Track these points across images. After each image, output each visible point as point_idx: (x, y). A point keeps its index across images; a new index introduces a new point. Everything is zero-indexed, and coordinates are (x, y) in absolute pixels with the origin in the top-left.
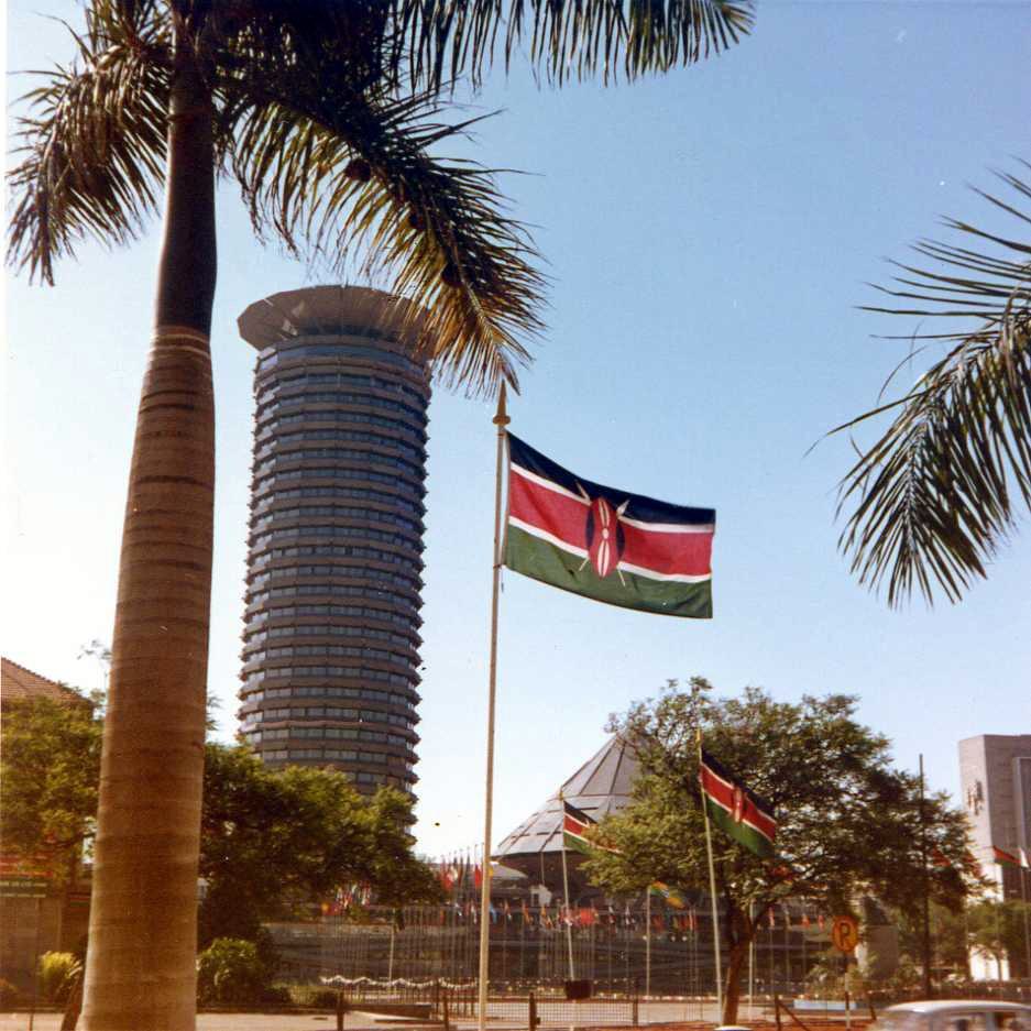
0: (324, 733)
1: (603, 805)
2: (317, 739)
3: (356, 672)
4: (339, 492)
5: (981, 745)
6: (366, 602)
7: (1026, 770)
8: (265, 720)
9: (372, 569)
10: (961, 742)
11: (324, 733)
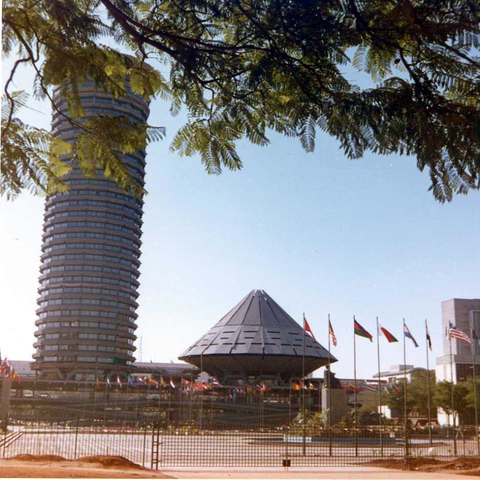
0: (80, 313)
1: (237, 330)
2: (78, 293)
3: (101, 258)
4: (90, 203)
5: (453, 303)
6: (105, 241)
7: (477, 317)
8: (50, 283)
9: (110, 202)
10: (443, 303)
11: (80, 313)
